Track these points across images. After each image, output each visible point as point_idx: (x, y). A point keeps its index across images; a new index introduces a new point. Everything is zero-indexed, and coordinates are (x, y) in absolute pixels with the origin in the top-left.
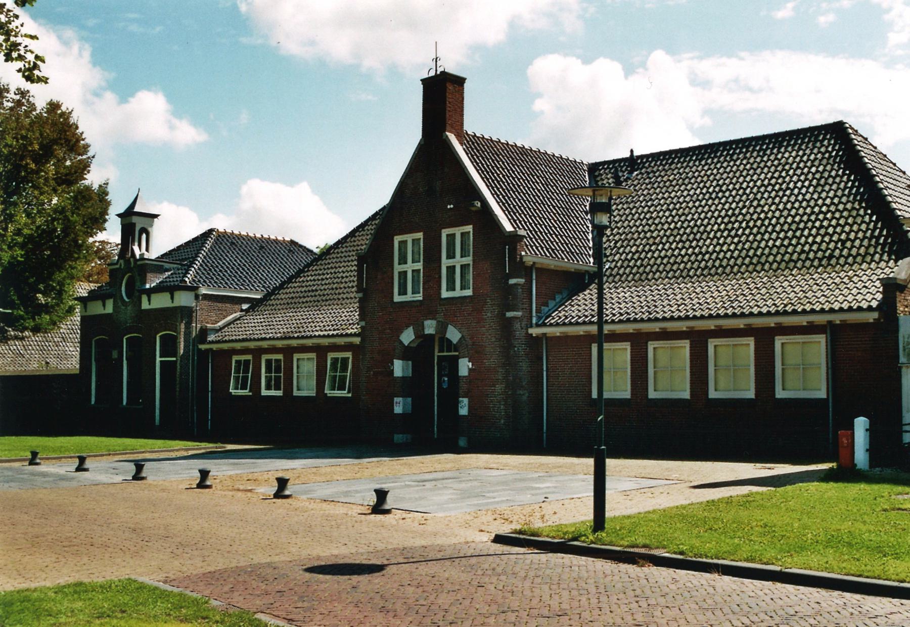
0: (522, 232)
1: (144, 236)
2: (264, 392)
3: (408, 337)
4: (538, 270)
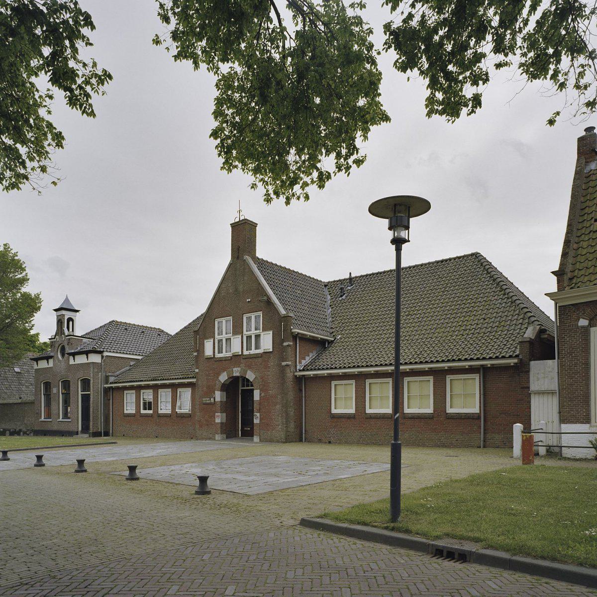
0: (291, 315)
1: (71, 323)
2: (143, 412)
3: (223, 378)
4: (300, 338)
